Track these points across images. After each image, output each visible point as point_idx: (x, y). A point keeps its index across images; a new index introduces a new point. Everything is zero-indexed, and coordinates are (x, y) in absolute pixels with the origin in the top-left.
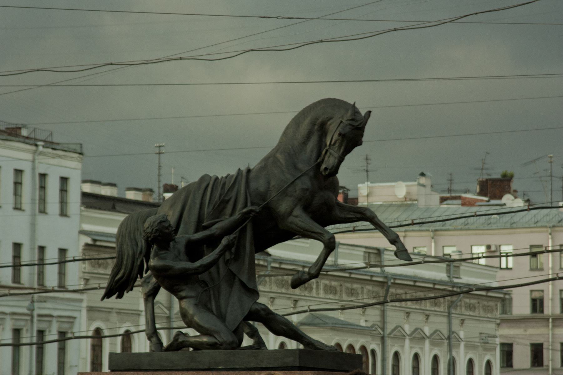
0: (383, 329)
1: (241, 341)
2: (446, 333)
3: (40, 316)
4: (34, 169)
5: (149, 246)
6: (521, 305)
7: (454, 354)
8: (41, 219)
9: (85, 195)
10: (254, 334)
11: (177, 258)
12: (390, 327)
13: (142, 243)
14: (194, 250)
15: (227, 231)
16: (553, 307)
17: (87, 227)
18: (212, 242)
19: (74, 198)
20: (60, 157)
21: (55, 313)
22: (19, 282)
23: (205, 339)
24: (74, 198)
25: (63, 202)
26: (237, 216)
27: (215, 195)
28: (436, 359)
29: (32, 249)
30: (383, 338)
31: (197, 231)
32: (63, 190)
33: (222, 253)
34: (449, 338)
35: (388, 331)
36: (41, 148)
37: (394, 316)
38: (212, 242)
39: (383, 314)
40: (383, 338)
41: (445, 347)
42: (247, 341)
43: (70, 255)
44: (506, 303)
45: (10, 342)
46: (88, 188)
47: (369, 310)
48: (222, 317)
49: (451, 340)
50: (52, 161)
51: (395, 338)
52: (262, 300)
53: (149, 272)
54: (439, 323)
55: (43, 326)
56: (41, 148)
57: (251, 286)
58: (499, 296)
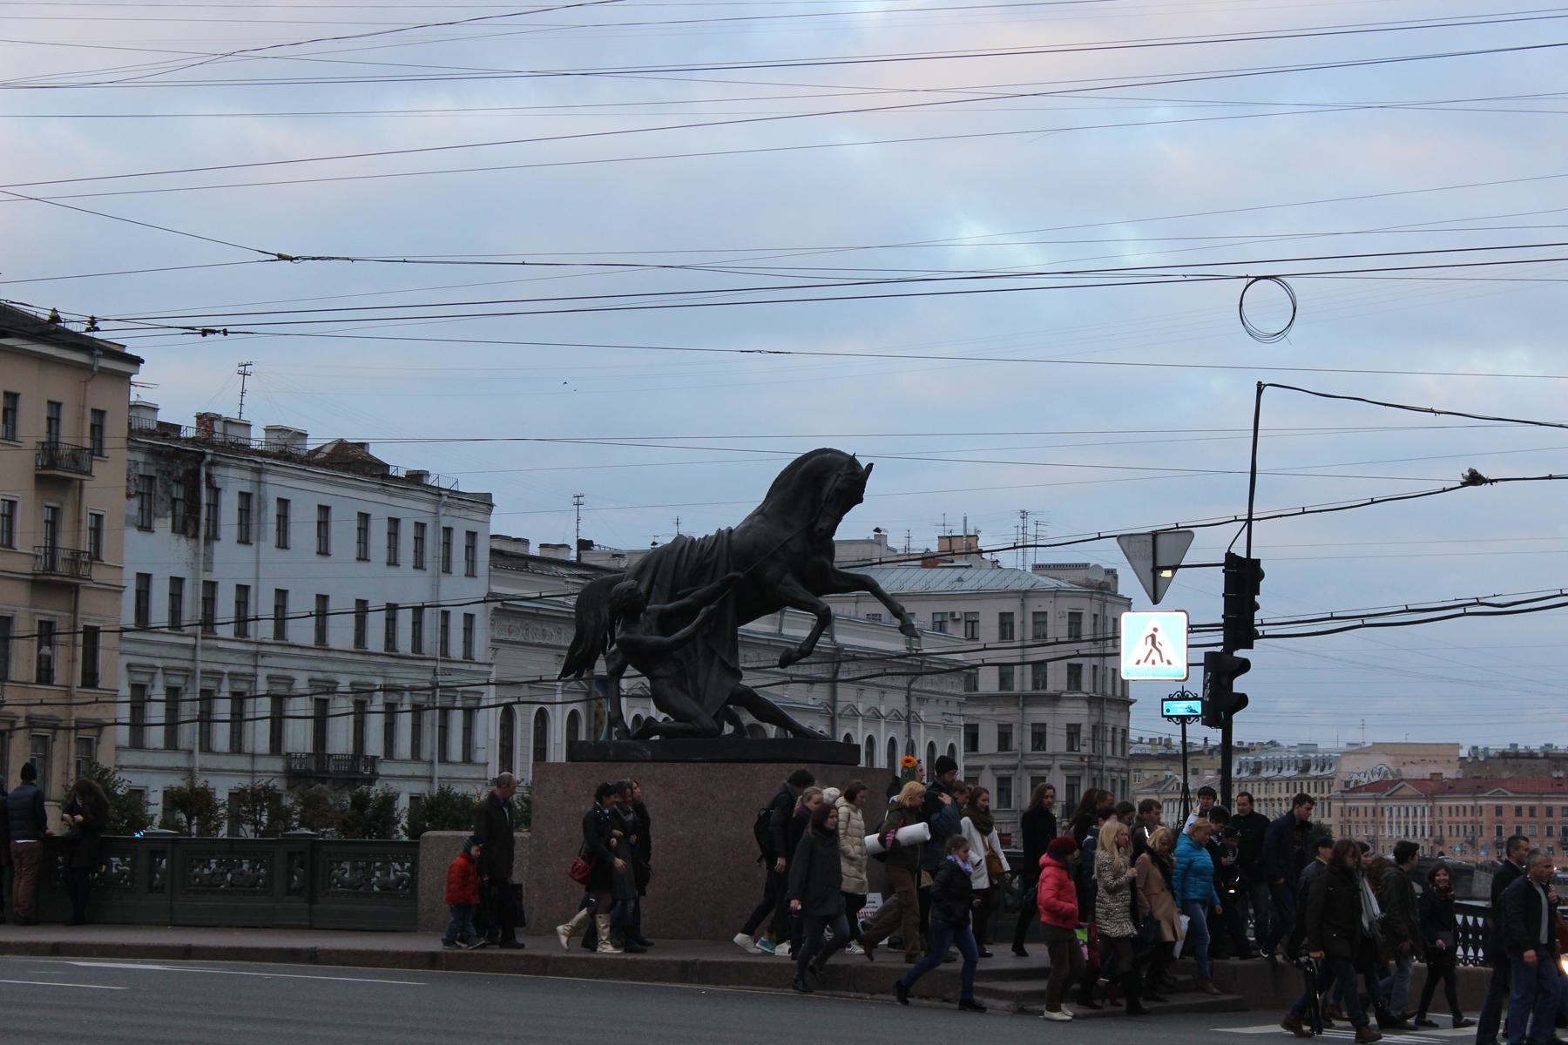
0: (833, 708)
1: (722, 728)
2: (904, 713)
3: (203, 672)
4: (437, 522)
5: (614, 616)
6: (988, 682)
7: (913, 737)
8: (445, 580)
9: (493, 552)
10: (734, 720)
11: (648, 631)
12: (840, 707)
13: (605, 612)
14: (667, 622)
15: (704, 601)
16: (1023, 683)
17: (496, 589)
18: (686, 614)
19: (483, 556)
20: (467, 508)
21: (159, 663)
22: (394, 650)
23: (681, 725)
24: (483, 556)
25: (393, 547)
26: (715, 584)
27: (682, 565)
28: (892, 742)
29: (195, 584)
30: (833, 720)
31: (670, 601)
32: (419, 540)
33: (699, 627)
34: (908, 719)
35: (839, 710)
36: (445, 499)
37: (846, 694)
38: (686, 614)
39: (834, 693)
40: (833, 720)
41: (903, 729)
42: (728, 729)
43: (333, 606)
44: (971, 683)
45: (228, 717)
46: (497, 545)
47: (817, 687)
48: (699, 699)
49: (910, 720)
50: (456, 512)
51: (847, 717)
52: (748, 681)
53: (614, 647)
54: (896, 701)
55: (211, 684)
56: (445, 499)
57: (732, 665)
58: (968, 674)
